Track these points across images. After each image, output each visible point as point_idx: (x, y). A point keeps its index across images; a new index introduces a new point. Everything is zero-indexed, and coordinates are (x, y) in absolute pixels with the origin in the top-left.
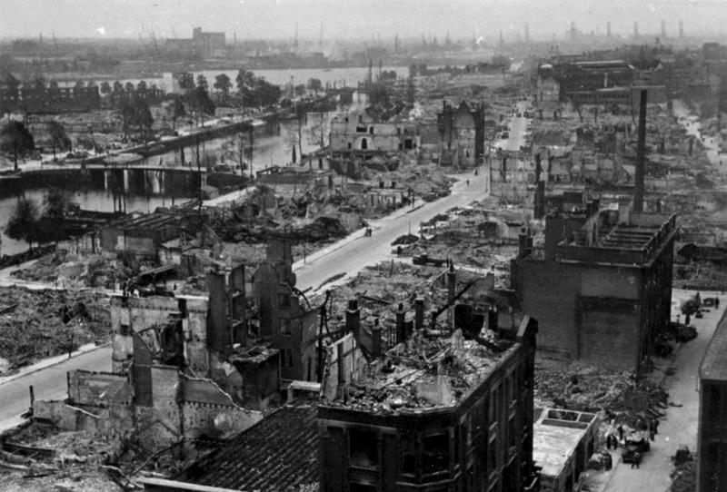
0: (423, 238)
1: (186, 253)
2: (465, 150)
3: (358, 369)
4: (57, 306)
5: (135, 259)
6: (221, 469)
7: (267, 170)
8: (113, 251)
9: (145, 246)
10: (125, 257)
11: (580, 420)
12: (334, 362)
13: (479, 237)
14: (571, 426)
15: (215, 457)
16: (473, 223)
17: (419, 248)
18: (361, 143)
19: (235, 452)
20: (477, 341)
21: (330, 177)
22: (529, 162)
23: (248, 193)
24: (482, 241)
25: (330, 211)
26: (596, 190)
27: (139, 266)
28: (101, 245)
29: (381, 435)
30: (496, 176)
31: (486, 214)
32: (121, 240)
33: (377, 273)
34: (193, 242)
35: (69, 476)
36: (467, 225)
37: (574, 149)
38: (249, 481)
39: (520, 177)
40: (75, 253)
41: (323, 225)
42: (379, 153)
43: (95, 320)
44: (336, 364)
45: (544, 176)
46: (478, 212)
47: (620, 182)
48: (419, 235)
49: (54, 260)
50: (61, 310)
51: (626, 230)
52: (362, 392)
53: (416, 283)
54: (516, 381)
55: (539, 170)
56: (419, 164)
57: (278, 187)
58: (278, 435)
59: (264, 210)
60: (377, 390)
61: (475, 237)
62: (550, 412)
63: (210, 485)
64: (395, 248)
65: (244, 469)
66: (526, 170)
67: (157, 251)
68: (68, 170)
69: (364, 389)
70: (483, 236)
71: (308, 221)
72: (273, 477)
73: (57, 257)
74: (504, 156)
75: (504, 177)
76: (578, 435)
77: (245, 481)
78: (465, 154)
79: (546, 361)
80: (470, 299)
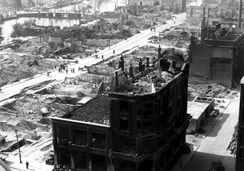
0: (160, 37)
1: (73, 43)
2: (178, 6)
3: (123, 81)
4: (27, 61)
5: (55, 45)
6: (78, 115)
7: (105, 13)
8: (48, 42)
9: (58, 40)
10: (52, 45)
11: (208, 100)
12: (114, 78)
13: (180, 37)
14: (205, 102)
15: (76, 111)
16: (179, 32)
17: (158, 41)
18: (140, 3)
19: (83, 109)
20: (167, 72)
21: (127, 15)
22: (201, 10)
23: (97, 21)
24: (182, 39)
25: (126, 28)
26: (225, 21)
27: (57, 48)
28: (43, 40)
29: (130, 103)
30: (189, 15)
31: (184, 29)
32: (50, 38)
33: (141, 49)
34: (75, 39)
35: (30, 118)
36: (177, 33)
37: (219, 5)
38: (87, 119)
39: (197, 16)
40: (34, 42)
41: (123, 32)
42: (146, 6)
43: (41, 66)
44: (115, 79)
45: (206, 16)
46: (181, 28)
47: (234, 18)
48: (158, 36)
49: (27, 45)
50: (29, 62)
51: (232, 34)
52: (124, 89)
53: (155, 53)
54: (181, 85)
55: (204, 13)
56: (161, 11)
57: (108, 19)
58: (98, 104)
59: (102, 28)
60: (129, 88)
61: (179, 37)
62: (198, 98)
63: (74, 120)
64: (150, 41)
65: (86, 115)
66: (200, 13)
67: (63, 42)
68: (33, 14)
69: (125, 87)
70: (182, 37)
71: (118, 31)
72: (95, 117)
73: (28, 44)
74: (192, 8)
75: (192, 16)
76: (206, 105)
77: (86, 118)
78: (178, 7)
79: (199, 81)
80: (166, 57)
